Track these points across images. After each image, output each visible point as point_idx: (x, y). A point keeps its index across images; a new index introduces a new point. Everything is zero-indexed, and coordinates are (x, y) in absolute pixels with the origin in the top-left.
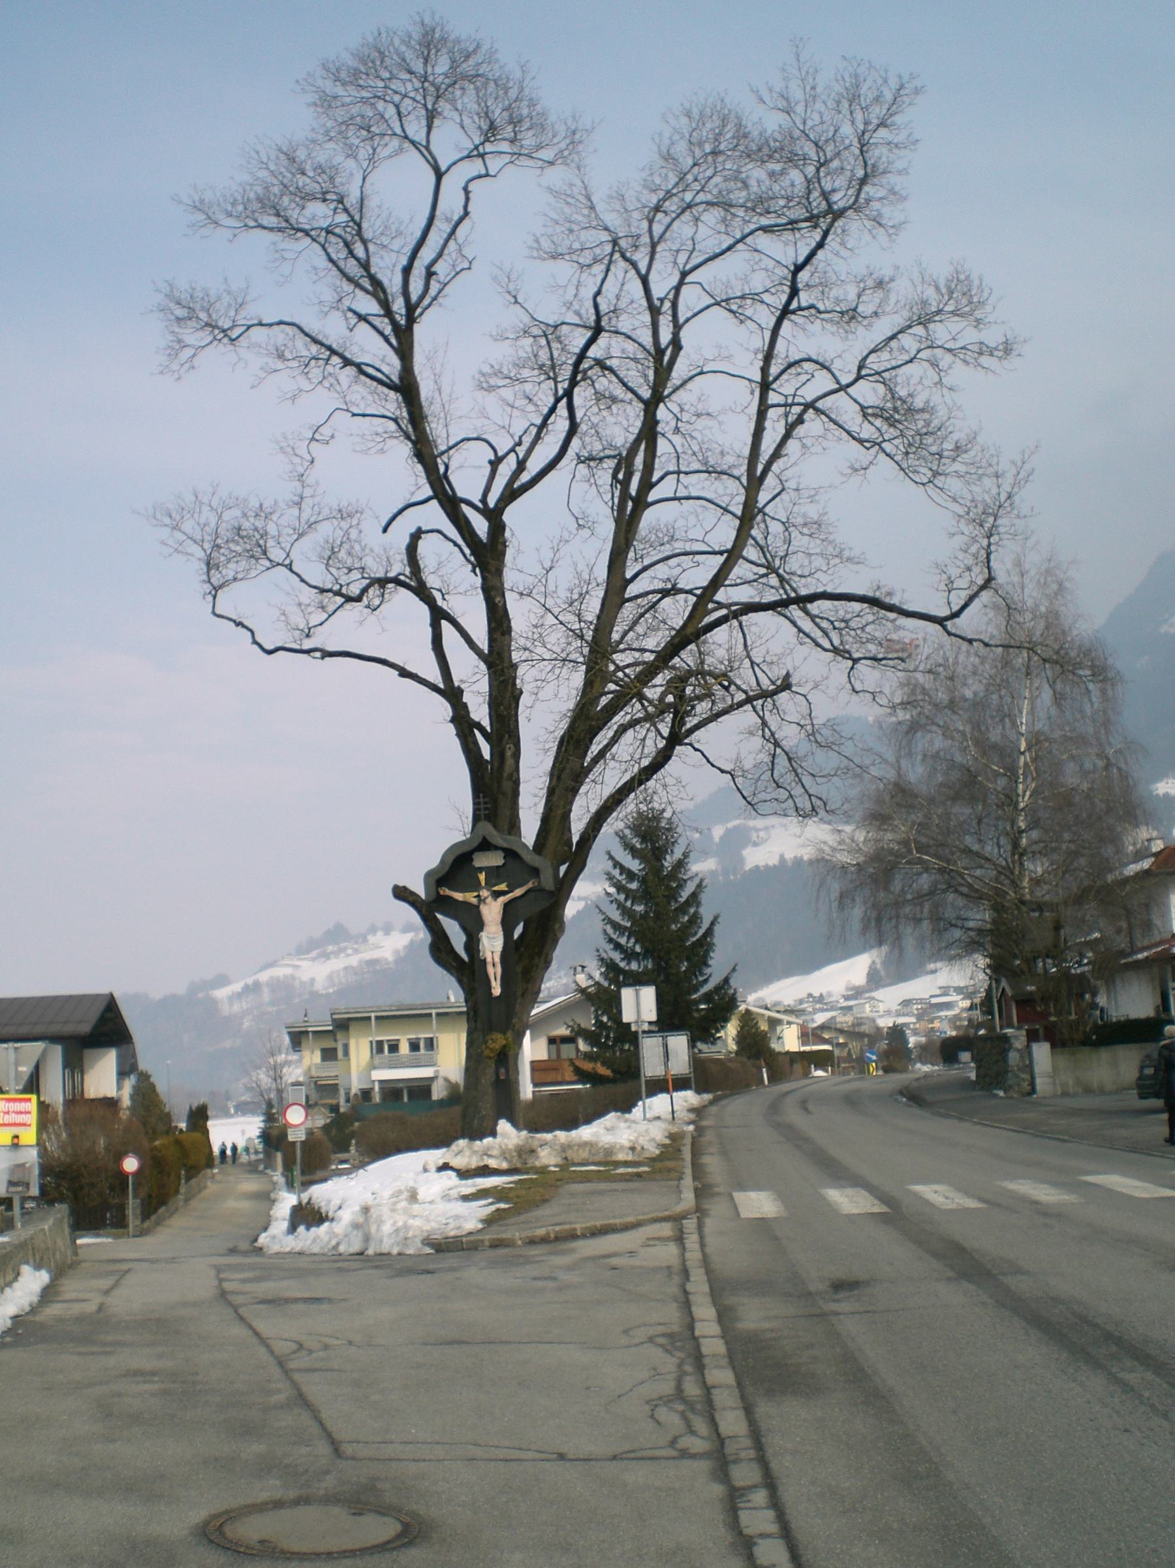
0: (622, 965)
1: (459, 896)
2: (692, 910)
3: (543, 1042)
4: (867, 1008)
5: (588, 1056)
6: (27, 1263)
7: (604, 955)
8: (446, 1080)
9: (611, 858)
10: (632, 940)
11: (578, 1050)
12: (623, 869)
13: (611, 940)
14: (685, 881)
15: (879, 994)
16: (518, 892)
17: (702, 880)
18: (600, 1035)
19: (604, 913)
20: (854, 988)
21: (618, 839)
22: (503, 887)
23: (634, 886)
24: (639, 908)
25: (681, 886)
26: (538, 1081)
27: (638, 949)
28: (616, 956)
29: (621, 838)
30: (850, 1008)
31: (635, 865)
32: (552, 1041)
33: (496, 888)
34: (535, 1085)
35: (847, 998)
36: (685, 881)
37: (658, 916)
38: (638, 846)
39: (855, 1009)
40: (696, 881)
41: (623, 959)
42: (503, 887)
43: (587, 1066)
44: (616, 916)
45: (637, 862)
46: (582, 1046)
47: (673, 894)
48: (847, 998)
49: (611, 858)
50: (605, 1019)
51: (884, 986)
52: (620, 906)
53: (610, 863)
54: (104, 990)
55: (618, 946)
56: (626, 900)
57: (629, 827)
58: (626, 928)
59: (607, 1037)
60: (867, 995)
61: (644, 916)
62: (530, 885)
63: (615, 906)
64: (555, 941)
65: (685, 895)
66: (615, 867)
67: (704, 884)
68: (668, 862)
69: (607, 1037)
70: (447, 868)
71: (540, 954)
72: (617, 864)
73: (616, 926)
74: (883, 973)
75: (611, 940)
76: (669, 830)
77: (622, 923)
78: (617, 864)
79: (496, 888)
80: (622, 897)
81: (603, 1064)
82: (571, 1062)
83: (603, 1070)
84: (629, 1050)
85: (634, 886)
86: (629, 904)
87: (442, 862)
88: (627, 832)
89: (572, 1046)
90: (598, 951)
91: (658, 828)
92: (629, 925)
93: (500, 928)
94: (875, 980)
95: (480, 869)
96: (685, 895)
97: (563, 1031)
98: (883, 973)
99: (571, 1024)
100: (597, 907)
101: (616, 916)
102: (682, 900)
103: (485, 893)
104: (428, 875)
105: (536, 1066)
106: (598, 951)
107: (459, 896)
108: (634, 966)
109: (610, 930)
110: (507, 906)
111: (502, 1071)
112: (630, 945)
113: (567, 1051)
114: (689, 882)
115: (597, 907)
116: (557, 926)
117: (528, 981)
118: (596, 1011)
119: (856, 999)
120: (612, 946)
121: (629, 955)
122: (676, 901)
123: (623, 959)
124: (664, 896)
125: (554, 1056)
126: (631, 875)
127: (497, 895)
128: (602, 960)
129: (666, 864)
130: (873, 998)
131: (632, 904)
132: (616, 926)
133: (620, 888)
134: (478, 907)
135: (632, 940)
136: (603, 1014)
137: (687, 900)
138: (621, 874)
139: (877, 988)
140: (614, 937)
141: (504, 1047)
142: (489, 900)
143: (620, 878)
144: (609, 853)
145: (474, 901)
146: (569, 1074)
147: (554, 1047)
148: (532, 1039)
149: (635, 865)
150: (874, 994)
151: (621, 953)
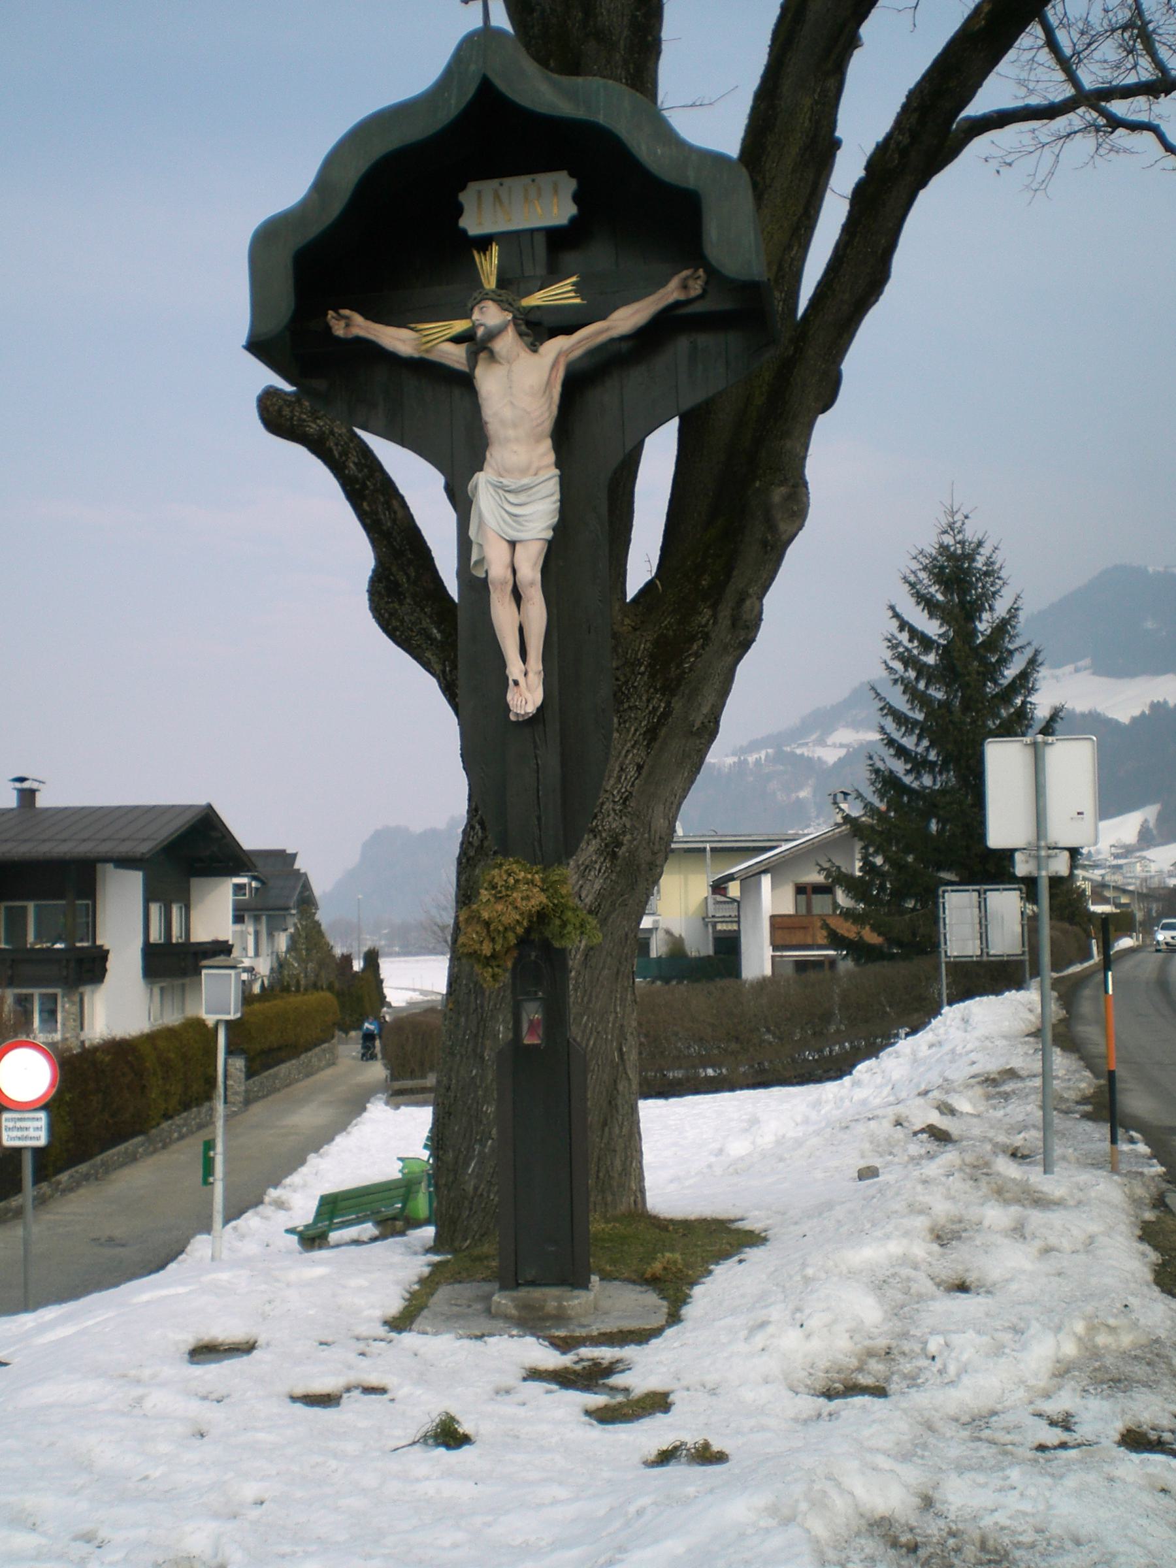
0: (907, 780)
1: (399, 340)
2: (1018, 701)
3: (788, 892)
4: (1138, 867)
5: (848, 914)
6: (841, 886)
7: (880, 765)
8: (668, 932)
9: (896, 615)
10: (925, 743)
11: (836, 905)
12: (914, 633)
13: (891, 742)
14: (1011, 653)
15: (1151, 853)
16: (626, 319)
17: (1037, 653)
18: (870, 884)
19: (882, 699)
20: (1124, 846)
21: (906, 587)
22: (560, 294)
23: (931, 659)
24: (938, 694)
25: (1003, 661)
26: (779, 942)
27: (932, 756)
28: (899, 767)
29: (912, 585)
30: (1119, 867)
31: (932, 628)
32: (800, 890)
33: (537, 299)
34: (775, 948)
35: (1116, 856)
36: (1011, 653)
37: (966, 707)
38: (940, 597)
39: (1124, 870)
40: (1028, 653)
41: (908, 772)
42: (560, 294)
43: (848, 930)
44: (901, 702)
45: (936, 623)
46: (842, 898)
47: (991, 672)
48: (1116, 856)
49: (896, 615)
50: (879, 861)
51: (1156, 846)
52: (909, 689)
53: (895, 623)
54: (202, 801)
55: (901, 752)
56: (917, 679)
57: (925, 569)
58: (916, 723)
59: (882, 888)
60: (1138, 854)
61: (945, 705)
62: (671, 292)
63: (900, 688)
64: (773, 553)
65: (1010, 672)
66: (901, 629)
67: (1040, 659)
68: (984, 625)
69: (882, 888)
70: (336, 208)
71: (714, 596)
72: (903, 625)
73: (900, 719)
74: (1155, 832)
75: (891, 742)
76: (987, 574)
77: (910, 714)
78: (903, 625)
79: (537, 299)
80: (912, 674)
81: (874, 928)
82: (823, 918)
83: (871, 937)
84: (913, 910)
85: (931, 659)
86: (921, 685)
87: (322, 185)
88: (923, 575)
89: (827, 898)
90: (871, 758)
91: (969, 571)
92: (920, 716)
93: (544, 453)
94: (1147, 838)
95: (483, 243)
96: (1010, 672)
97: (818, 878)
98: (1155, 832)
99: (827, 865)
100: (873, 688)
101: (901, 702)
102: (1005, 682)
103: (490, 315)
104: (267, 238)
105: (777, 922)
106: (871, 758)
107: (399, 340)
108: (927, 780)
109: (890, 725)
110: (577, 385)
111: (533, 1013)
112: (920, 750)
113: (821, 904)
114: (1017, 655)
115: (873, 688)
116: (778, 494)
117: (669, 689)
118: (865, 848)
119: (1126, 857)
120: (892, 751)
121: (919, 765)
122: (995, 683)
123: (908, 772)
124: (978, 673)
125: (803, 911)
126: (926, 643)
127: (538, 328)
128: (877, 771)
129: (981, 627)
130: (1144, 858)
131: (927, 686)
132: (900, 719)
133: (908, 660)
134: (465, 382)
135: (925, 743)
136: (876, 853)
137: (1014, 681)
138: (911, 641)
139: (1148, 848)
140: (896, 735)
141: (541, 917)
142: (507, 343)
143: (910, 646)
144: (892, 608)
145: (454, 355)
146: (821, 937)
147: (803, 897)
148: (774, 886)
149: (932, 628)
150: (1144, 853)
151: (906, 762)
